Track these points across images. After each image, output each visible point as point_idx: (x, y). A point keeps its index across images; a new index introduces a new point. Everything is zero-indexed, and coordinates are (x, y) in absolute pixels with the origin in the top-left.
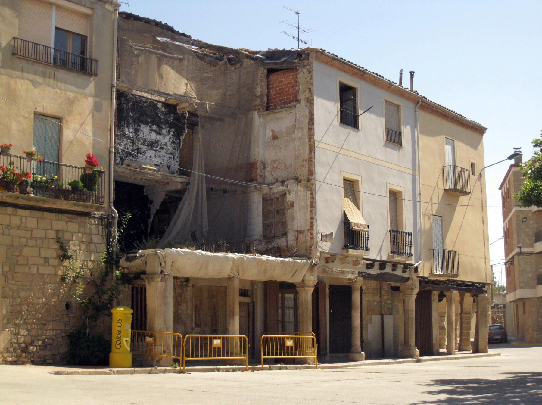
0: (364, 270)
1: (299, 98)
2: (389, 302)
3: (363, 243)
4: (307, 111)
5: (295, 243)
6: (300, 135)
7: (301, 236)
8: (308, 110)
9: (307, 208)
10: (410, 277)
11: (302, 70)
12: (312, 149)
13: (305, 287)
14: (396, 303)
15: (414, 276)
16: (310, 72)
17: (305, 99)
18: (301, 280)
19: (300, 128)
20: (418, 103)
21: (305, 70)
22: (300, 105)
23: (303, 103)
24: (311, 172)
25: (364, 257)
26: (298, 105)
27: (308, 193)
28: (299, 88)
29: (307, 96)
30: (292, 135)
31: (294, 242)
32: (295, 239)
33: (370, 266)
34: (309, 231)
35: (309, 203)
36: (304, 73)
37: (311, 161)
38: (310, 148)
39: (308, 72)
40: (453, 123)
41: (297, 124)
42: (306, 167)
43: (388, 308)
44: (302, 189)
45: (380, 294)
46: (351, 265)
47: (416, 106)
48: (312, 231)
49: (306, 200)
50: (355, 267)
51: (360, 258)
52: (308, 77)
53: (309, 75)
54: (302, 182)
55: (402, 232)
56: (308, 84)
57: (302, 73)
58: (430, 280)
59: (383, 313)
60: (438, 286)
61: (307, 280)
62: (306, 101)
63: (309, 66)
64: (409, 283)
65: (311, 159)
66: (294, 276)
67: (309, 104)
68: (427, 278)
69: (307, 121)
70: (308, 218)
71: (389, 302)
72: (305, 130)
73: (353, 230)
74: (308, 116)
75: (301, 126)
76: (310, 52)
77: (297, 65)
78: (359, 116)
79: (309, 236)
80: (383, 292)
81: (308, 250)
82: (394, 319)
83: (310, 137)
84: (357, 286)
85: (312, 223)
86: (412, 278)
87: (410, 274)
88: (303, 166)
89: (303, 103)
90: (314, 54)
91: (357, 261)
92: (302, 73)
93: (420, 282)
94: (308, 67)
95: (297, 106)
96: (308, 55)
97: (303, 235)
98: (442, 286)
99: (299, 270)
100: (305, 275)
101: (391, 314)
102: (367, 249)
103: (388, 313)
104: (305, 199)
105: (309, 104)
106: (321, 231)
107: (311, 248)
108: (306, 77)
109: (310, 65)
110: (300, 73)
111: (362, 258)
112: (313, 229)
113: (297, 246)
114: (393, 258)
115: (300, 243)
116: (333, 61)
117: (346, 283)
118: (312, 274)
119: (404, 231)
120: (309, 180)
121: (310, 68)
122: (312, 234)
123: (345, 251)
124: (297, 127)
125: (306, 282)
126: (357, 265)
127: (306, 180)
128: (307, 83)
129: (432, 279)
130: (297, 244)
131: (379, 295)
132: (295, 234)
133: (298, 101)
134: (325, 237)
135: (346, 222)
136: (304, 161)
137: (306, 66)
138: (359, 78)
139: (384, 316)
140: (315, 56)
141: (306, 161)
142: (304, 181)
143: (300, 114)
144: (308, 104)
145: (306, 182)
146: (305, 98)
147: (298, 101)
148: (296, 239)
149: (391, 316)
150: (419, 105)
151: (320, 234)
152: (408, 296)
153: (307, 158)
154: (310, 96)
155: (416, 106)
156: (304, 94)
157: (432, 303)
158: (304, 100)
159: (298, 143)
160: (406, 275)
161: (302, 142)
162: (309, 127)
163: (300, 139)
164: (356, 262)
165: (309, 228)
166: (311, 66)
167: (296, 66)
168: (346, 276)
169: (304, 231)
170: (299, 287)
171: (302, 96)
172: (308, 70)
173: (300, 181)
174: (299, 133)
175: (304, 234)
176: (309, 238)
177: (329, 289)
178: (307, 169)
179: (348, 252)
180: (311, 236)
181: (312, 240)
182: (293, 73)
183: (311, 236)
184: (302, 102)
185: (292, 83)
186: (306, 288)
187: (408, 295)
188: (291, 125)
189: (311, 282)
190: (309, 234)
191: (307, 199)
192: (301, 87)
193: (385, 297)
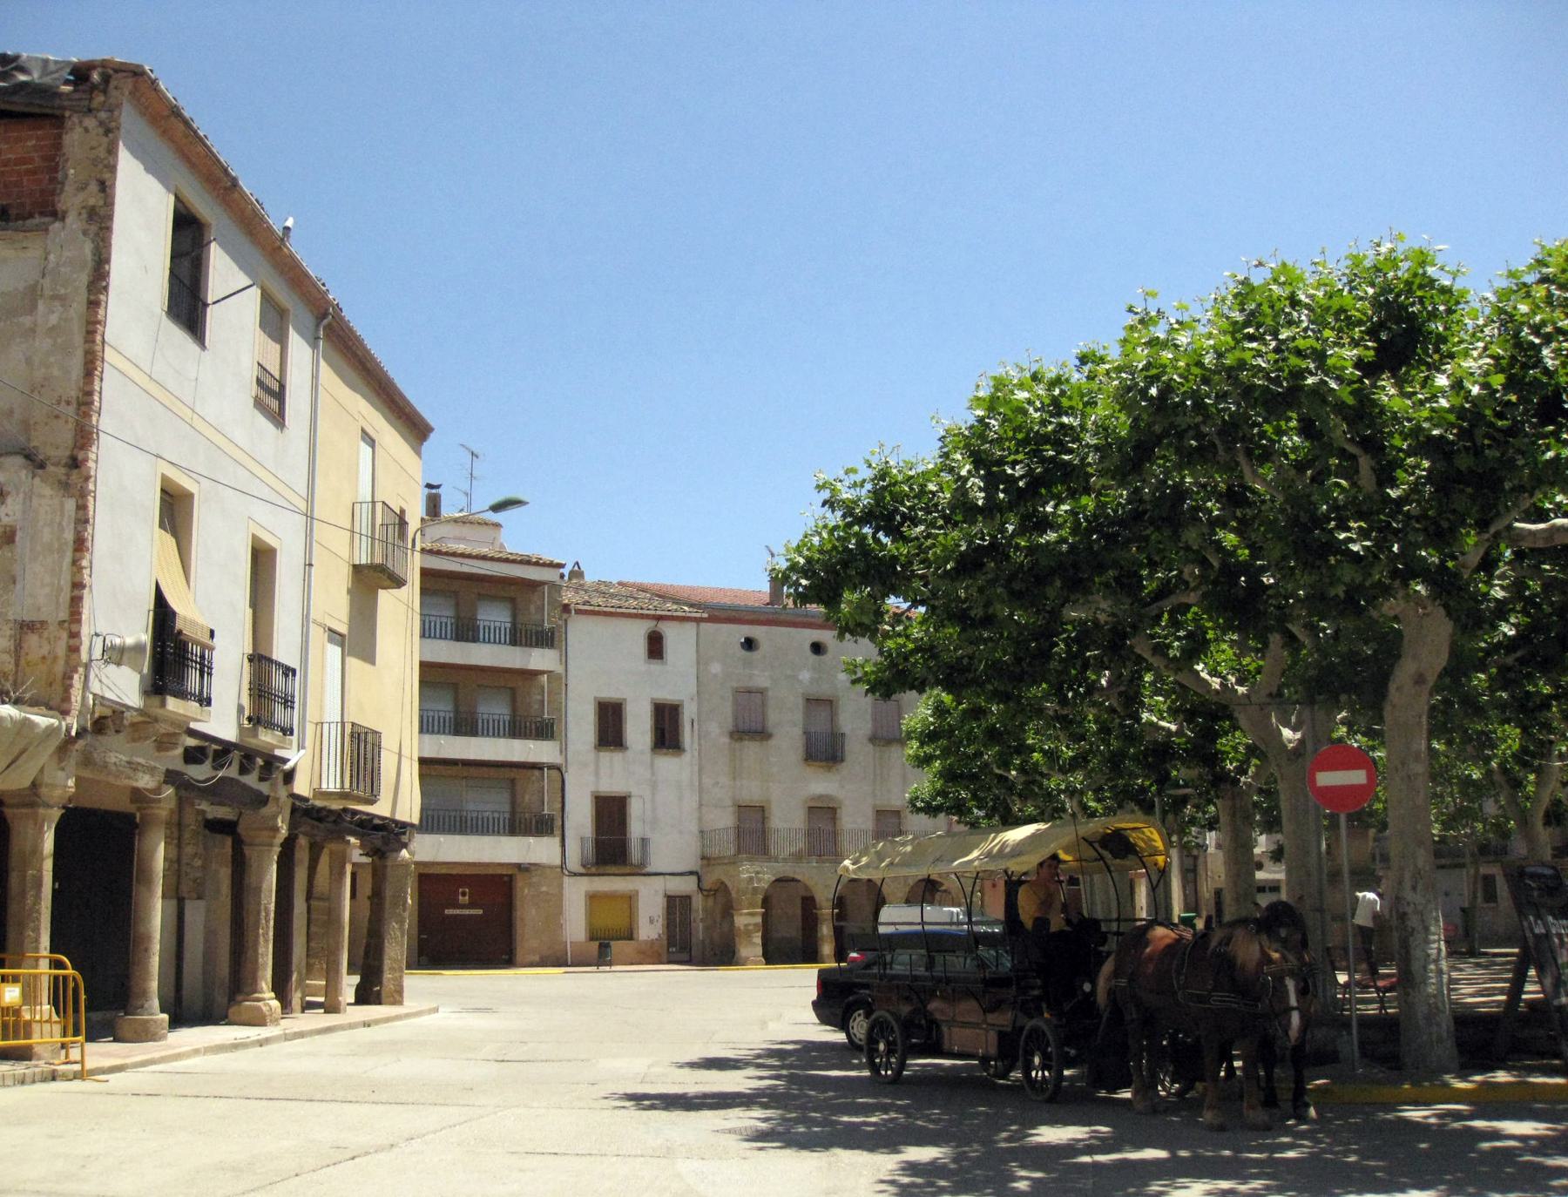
0: (179, 765)
1: (60, 207)
2: (198, 863)
3: (193, 680)
4: (88, 248)
5: (13, 661)
6: (54, 319)
7: (32, 640)
8: (92, 246)
9: (61, 551)
10: (272, 794)
11: (81, 122)
12: (91, 365)
13: (39, 806)
14: (214, 866)
15: (282, 793)
16: (108, 131)
17: (84, 211)
18: (27, 783)
19: (55, 297)
20: (325, 315)
21: (90, 122)
22: (63, 228)
23: (74, 222)
24: (84, 436)
25: (193, 725)
26: (57, 225)
27: (70, 505)
28: (66, 176)
29: (92, 202)
30: (21, 319)
31: (6, 657)
32: (12, 648)
33: (192, 756)
34: (66, 625)
35: (69, 536)
36: (86, 130)
37: (85, 402)
38: (86, 364)
39: (101, 130)
40: (379, 395)
41: (47, 282)
42: (67, 422)
43: (195, 881)
44: (47, 491)
45: (179, 839)
46: (149, 744)
47: (317, 326)
48: (74, 628)
49: (60, 524)
50: (162, 753)
51: (179, 726)
52: (100, 145)
53: (105, 140)
54: (50, 468)
55: (270, 661)
56: (100, 166)
57: (79, 130)
58: (313, 807)
59: (185, 895)
60: (322, 826)
61: (47, 785)
62: (84, 216)
63: (109, 113)
64: (267, 811)
65: (87, 399)
66: (13, 766)
67: (94, 228)
68: (306, 800)
69: (84, 278)
70: (62, 582)
71: (198, 863)
72: (75, 305)
73: (182, 637)
74: (90, 264)
75: (62, 291)
76: (111, 72)
77: (66, 103)
78: (208, 305)
79: (65, 641)
80: (187, 835)
81: (58, 688)
82: (208, 911)
83: (91, 328)
84: (156, 811)
85: (76, 602)
86: (277, 799)
87: (274, 786)
88: (57, 417)
89: (74, 222)
90: (129, 80)
91: (175, 734)
92: (79, 130)
93: (294, 810)
94: (103, 115)
95: (51, 228)
96: (106, 79)
97: (40, 637)
98: (329, 825)
99: (31, 749)
100: (42, 770)
101: (199, 898)
102: (205, 701)
103: (195, 896)
104: (57, 520)
105: (94, 228)
106: (102, 627)
107: (68, 682)
108: (94, 143)
109: (111, 111)
110: (71, 129)
111: (185, 728)
112: (79, 621)
113: (16, 672)
114: (256, 736)
115: (28, 664)
116: (172, 118)
117: (124, 805)
118: (63, 764)
119: (274, 658)
120: (75, 463)
121: (112, 119)
122: (75, 635)
123: (156, 700)
124: (48, 292)
125: (44, 791)
126: (167, 749)
127: (64, 462)
128: (95, 162)
129: (319, 803)
130: (17, 665)
131: (176, 841)
132: (13, 632)
133: (57, 215)
134: (116, 655)
135: (163, 614)
136: (63, 403)
137: (98, 110)
138: (218, 196)
139: (187, 902)
140: (130, 87)
141: (68, 403)
142: (56, 464)
143: (61, 256)
144: (92, 227)
145: (62, 471)
146: (83, 208)
147: (57, 215)
148: (16, 648)
149: (201, 903)
150: (325, 322)
151: (101, 638)
152: (261, 848)
153: (73, 393)
154: (101, 203)
155: (317, 326)
156: (81, 196)
157: (296, 869)
158: (80, 214)
159: (43, 343)
160: (264, 788)
161: (59, 340)
162: (92, 298)
163: (53, 330)
164: (165, 740)
165: (64, 615)
166: (116, 113)
167: (64, 108)
168: (137, 780)
169: (43, 623)
170: (13, 806)
171: (71, 200)
172: (101, 123)
173: (42, 466)
174: (53, 312)
175: (46, 634)
176: (61, 650)
177: (985, 932)
178: (71, 426)
179: (163, 704)
180: (72, 642)
181: (74, 656)
182: (39, 133)
183: (72, 642)
184: (70, 219)
185: (31, 161)
186: (41, 811)
187: (260, 845)
188: (21, 286)
189: (58, 792)
190: (65, 635)
191: (64, 524)
192: (72, 171)
193: (189, 850)
